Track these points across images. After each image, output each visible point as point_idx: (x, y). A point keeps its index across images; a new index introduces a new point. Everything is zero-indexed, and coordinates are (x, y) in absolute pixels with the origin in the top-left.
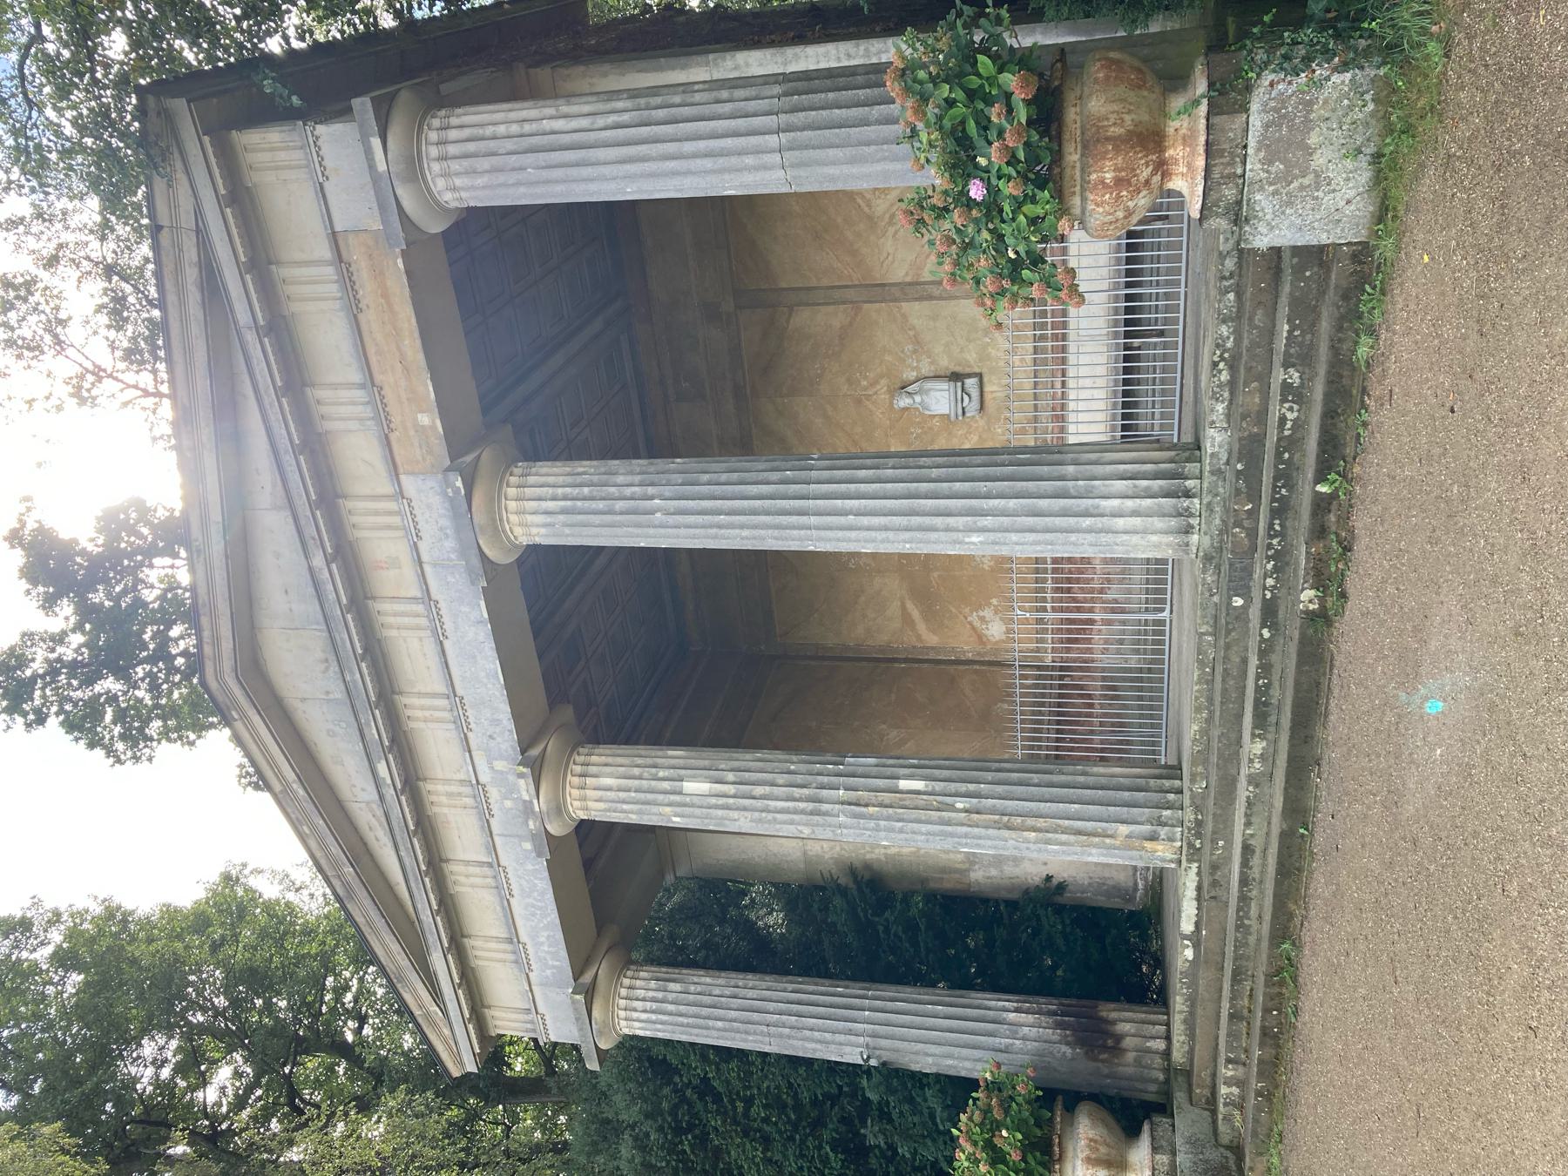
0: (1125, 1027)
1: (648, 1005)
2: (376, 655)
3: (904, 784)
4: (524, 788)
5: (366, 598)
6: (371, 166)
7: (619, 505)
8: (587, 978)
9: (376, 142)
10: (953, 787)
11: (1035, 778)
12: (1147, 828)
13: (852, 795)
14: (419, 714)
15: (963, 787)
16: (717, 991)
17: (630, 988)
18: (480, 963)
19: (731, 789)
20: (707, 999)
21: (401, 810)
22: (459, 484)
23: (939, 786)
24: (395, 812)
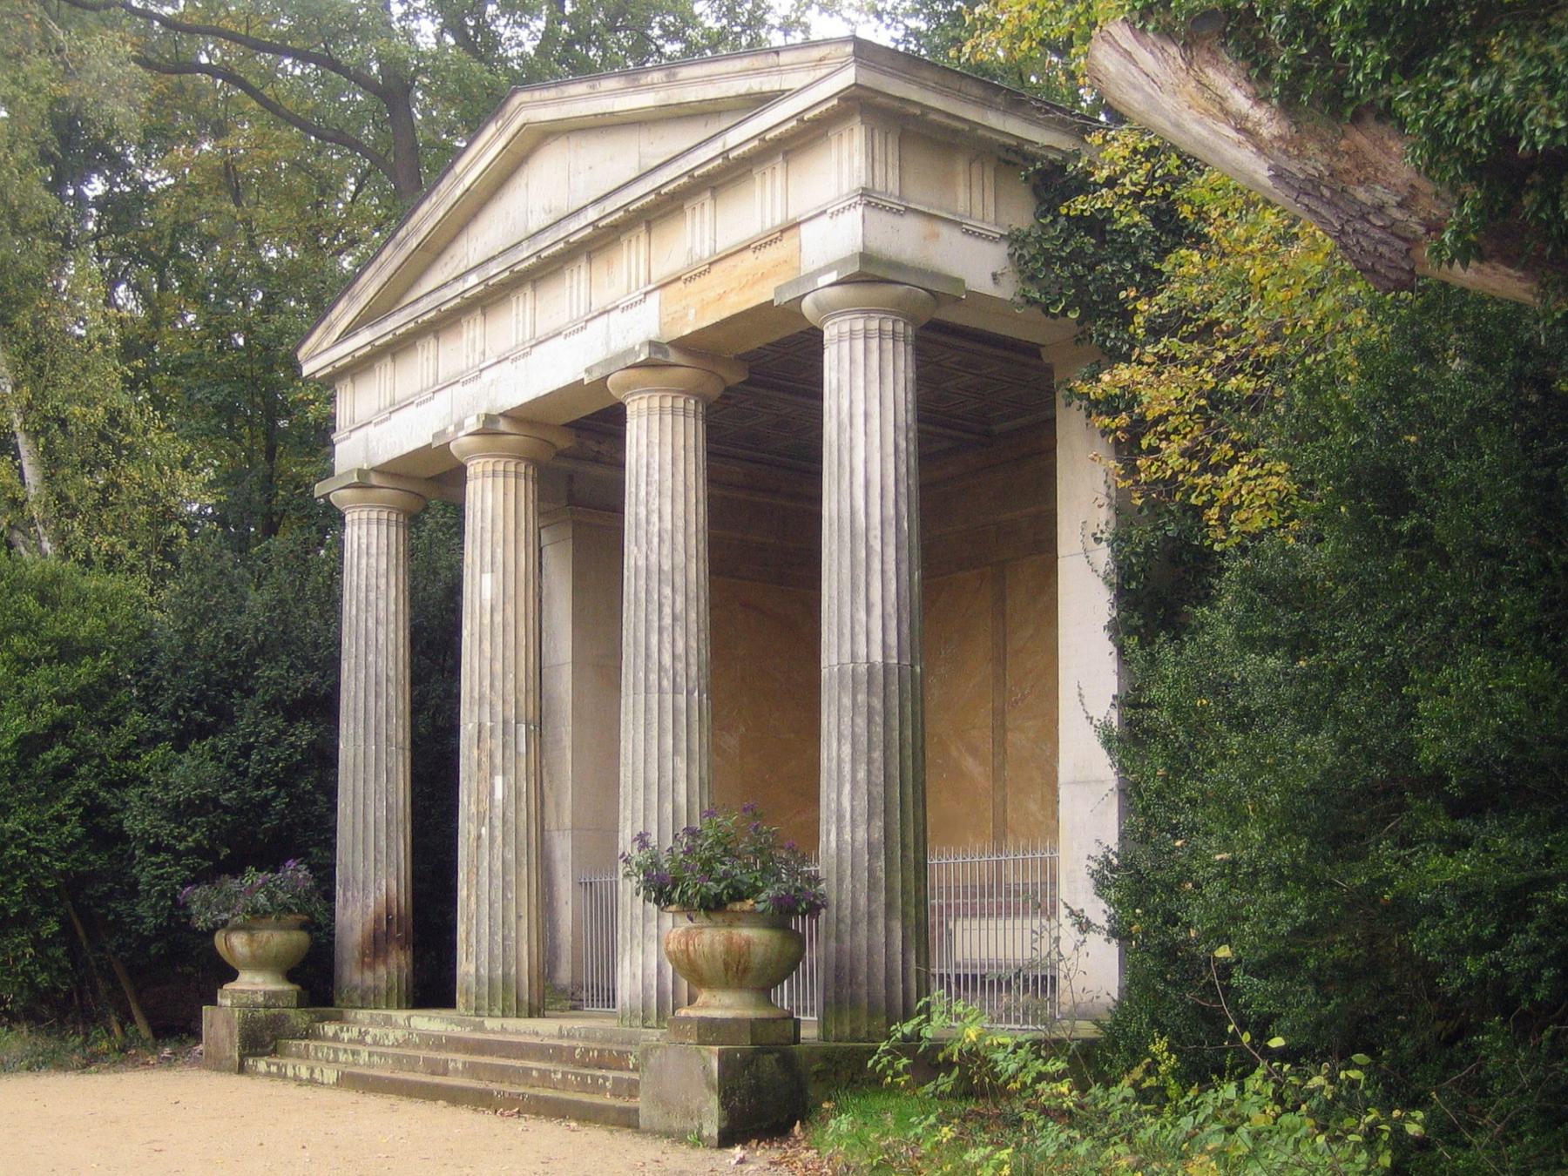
0: (382, 971)
1: (364, 541)
3: (498, 780)
4: (472, 424)
9: (833, 277)
10: (498, 823)
14: (845, 154)
16: (382, 604)
17: (378, 520)
18: (758, 189)
20: (372, 596)
22: (642, 357)
24: (448, 293)
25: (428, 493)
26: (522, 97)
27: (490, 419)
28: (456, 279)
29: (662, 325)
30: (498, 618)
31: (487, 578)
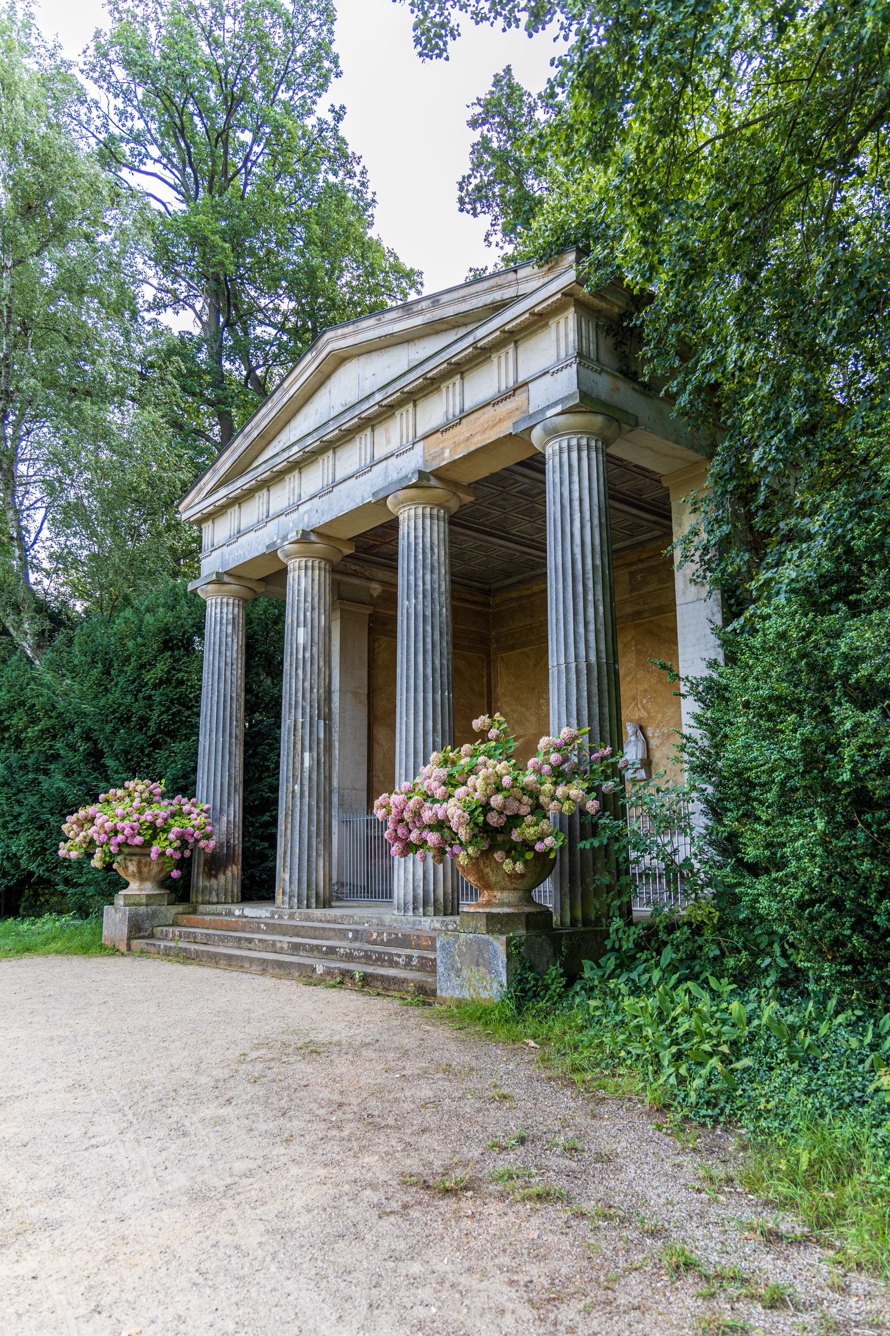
2: (347, 436)
3: (307, 755)
4: (293, 536)
5: (516, 342)
6: (549, 407)
7: (412, 578)
8: (226, 579)
9: (559, 409)
10: (306, 782)
11: (314, 829)
12: (288, 889)
13: (299, 726)
15: (306, 788)
18: (495, 360)
19: (300, 656)
21: (280, 463)
23: (306, 775)
24: (278, 460)
25: (262, 587)
26: (329, 335)
27: (305, 534)
28: (284, 450)
29: (425, 462)
30: (308, 655)
31: (301, 631)
